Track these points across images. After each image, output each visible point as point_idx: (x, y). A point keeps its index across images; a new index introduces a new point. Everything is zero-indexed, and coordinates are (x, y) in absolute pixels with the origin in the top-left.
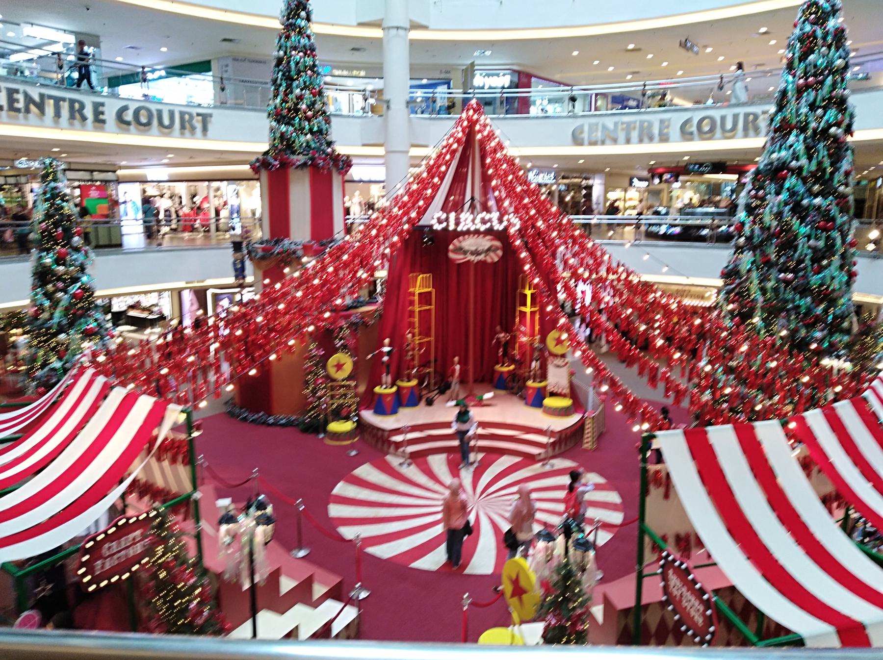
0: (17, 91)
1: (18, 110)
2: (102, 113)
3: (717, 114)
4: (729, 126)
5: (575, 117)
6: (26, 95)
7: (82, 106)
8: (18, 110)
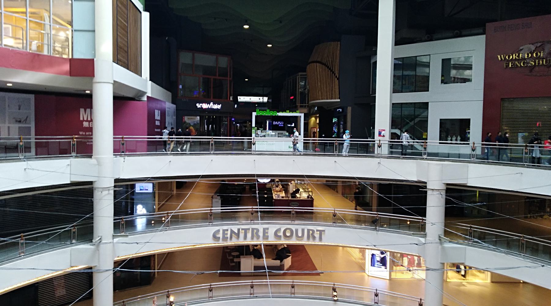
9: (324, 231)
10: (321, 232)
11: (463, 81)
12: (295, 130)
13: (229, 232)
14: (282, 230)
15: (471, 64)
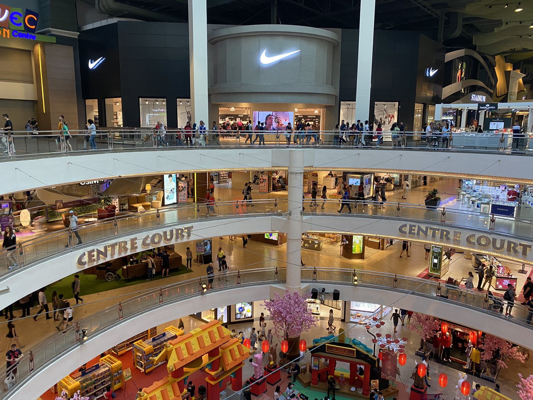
0: (93, 251)
6: (98, 250)
10: (525, 247)
13: (95, 253)
14: (477, 237)
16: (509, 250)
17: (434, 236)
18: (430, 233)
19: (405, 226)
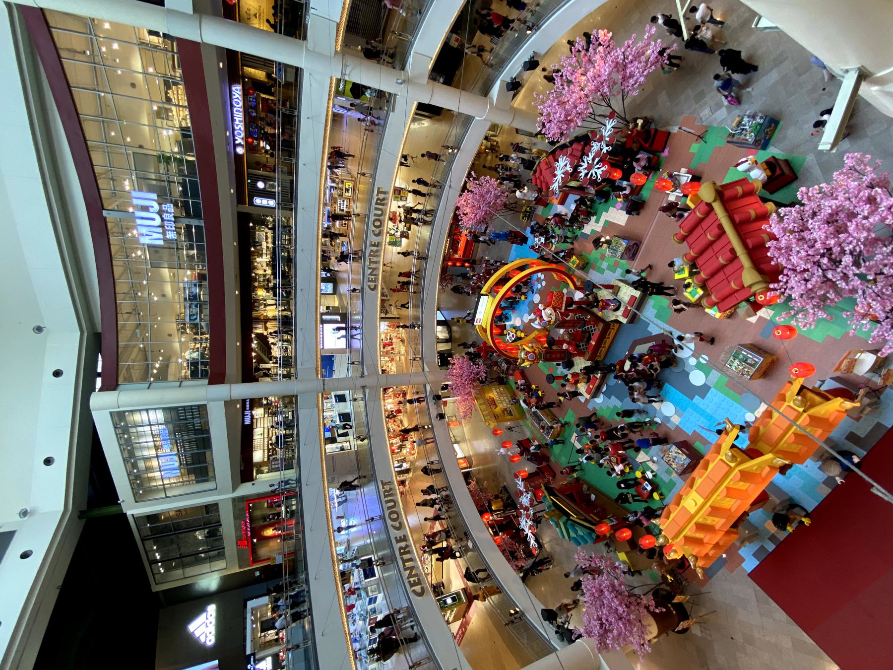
0: (410, 582)
1: (419, 579)
2: (400, 537)
3: (372, 218)
4: (380, 212)
5: (363, 289)
6: (408, 578)
7: (401, 548)
8: (419, 579)
9: (379, 188)
10: (379, 192)
11: (690, 470)
12: (149, 464)
13: (412, 579)
14: (374, 228)
15: (689, 517)
16: (383, 205)
17: (376, 262)
18: (373, 266)
19: (369, 286)
